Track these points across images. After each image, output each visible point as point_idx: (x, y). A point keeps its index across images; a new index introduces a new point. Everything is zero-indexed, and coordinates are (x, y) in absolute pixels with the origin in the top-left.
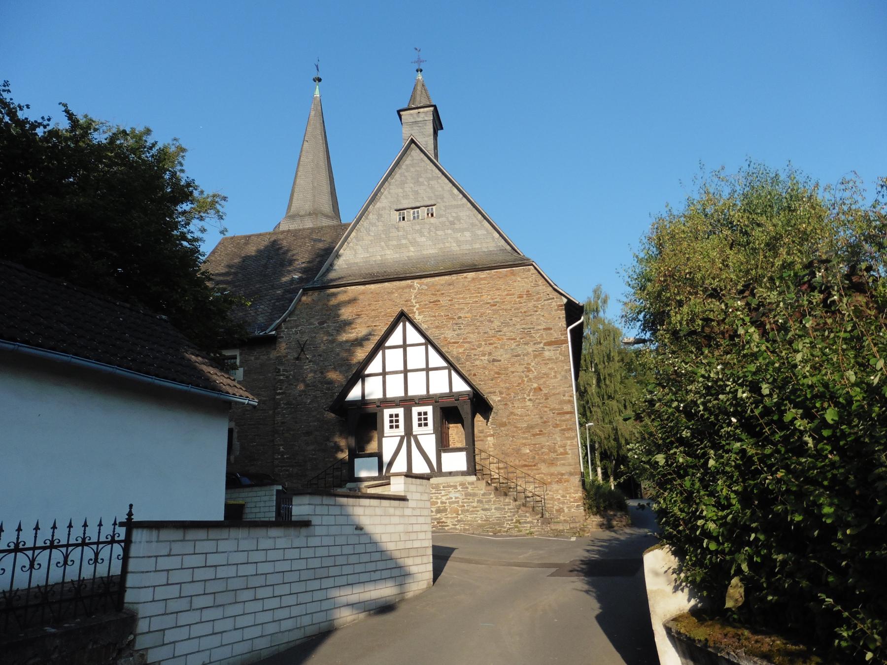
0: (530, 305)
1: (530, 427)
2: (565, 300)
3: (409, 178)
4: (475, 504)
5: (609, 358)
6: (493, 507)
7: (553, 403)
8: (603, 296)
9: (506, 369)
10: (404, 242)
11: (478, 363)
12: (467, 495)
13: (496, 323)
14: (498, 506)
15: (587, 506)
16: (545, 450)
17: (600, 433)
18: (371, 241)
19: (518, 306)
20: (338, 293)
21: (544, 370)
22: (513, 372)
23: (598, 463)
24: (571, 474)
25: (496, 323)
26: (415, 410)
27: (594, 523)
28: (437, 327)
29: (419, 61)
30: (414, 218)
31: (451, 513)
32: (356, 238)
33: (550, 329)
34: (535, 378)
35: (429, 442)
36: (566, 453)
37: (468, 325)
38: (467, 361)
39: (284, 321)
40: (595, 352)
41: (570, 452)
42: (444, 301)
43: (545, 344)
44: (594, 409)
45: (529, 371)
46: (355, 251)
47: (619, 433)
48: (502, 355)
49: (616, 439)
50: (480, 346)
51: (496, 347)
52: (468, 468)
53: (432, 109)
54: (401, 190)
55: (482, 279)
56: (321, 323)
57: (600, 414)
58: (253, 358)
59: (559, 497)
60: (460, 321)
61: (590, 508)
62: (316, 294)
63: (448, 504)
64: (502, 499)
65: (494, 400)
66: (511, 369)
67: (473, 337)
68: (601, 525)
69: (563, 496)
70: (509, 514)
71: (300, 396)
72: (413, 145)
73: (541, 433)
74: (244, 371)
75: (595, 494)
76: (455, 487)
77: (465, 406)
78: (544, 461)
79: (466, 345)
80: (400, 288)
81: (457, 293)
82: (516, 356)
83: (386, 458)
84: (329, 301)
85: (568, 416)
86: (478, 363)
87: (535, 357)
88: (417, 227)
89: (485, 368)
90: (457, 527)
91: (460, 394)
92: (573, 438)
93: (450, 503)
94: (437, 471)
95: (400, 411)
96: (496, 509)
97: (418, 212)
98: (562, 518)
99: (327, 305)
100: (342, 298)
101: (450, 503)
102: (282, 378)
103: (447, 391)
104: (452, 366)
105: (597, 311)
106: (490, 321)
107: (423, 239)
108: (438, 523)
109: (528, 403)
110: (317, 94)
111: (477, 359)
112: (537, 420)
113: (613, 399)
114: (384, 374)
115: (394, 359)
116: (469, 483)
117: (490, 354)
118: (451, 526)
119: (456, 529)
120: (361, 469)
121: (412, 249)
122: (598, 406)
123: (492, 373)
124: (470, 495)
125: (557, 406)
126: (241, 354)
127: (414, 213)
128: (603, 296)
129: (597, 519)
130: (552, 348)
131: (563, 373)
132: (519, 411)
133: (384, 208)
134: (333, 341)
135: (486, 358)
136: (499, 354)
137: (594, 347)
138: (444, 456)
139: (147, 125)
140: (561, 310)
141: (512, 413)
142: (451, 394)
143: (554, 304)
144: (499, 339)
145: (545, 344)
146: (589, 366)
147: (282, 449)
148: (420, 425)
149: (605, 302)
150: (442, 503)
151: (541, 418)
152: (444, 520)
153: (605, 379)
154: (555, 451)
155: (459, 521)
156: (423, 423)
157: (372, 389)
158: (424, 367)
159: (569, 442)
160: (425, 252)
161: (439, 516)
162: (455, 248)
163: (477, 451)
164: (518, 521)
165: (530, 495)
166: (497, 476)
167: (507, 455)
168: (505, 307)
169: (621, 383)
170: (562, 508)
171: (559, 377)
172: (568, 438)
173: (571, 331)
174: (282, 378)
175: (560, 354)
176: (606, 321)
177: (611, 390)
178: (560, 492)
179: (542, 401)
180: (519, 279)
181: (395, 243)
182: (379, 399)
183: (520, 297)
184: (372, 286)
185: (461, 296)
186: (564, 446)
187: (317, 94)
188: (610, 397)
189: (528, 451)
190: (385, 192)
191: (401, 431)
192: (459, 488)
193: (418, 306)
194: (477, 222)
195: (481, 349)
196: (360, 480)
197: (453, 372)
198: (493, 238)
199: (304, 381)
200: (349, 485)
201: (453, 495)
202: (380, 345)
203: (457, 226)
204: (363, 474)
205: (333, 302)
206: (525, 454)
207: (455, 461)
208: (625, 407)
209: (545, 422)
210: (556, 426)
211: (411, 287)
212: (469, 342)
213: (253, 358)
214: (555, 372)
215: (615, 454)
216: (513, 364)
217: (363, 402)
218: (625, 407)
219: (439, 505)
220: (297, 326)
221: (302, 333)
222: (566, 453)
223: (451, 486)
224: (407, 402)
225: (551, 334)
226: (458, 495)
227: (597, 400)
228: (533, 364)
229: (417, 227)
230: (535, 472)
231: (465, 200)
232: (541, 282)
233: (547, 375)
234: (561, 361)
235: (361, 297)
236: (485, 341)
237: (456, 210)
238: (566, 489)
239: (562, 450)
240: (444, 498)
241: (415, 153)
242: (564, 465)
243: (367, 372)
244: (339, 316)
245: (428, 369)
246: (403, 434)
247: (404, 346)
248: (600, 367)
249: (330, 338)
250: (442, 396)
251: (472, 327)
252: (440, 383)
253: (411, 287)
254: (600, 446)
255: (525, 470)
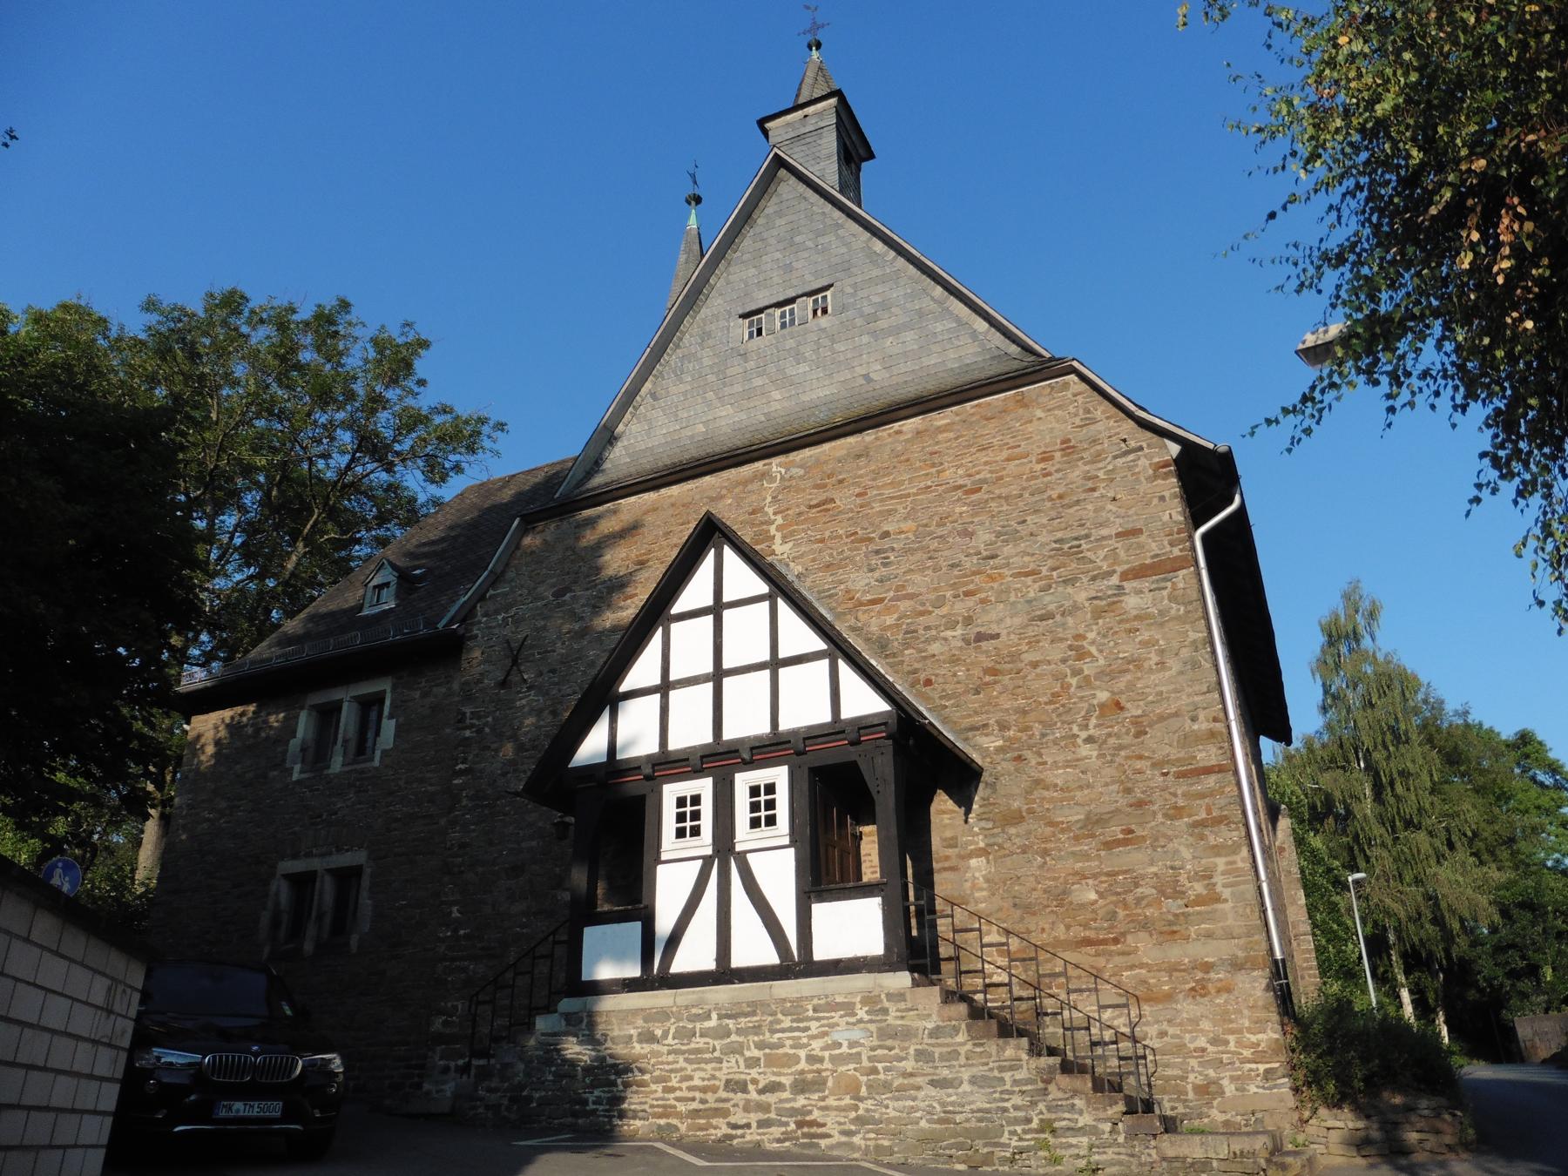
0: (1076, 474)
1: (1093, 822)
2: (1175, 449)
3: (773, 241)
4: (909, 1065)
5: (1399, 738)
6: (966, 1076)
7: (1160, 743)
8: (1365, 605)
9: (1015, 657)
10: (758, 382)
11: (935, 648)
12: (886, 1033)
13: (983, 537)
14: (979, 1070)
15: (1300, 1074)
16: (1145, 890)
17: (1396, 907)
18: (685, 393)
19: (1039, 483)
20: (599, 517)
21: (1128, 649)
22: (1035, 665)
23: (1401, 978)
24: (1237, 966)
25: (983, 537)
26: (743, 781)
27: (1334, 1136)
28: (828, 566)
29: (816, 27)
30: (783, 325)
31: (839, 1091)
32: (654, 396)
33: (1136, 532)
34: (1101, 674)
35: (777, 870)
36: (1218, 899)
37: (908, 551)
38: (907, 645)
39: (481, 598)
40: (1362, 723)
41: (1226, 893)
42: (844, 499)
43: (1125, 576)
44: (1374, 852)
45: (1080, 658)
46: (649, 421)
47: (1443, 905)
48: (1003, 620)
49: (1438, 921)
50: (940, 602)
51: (983, 601)
52: (887, 946)
53: (833, 101)
54: (753, 271)
55: (940, 430)
56: (559, 594)
57: (1388, 862)
58: (417, 694)
59: (1202, 1042)
60: (886, 544)
61: (1315, 1079)
62: (553, 526)
63: (827, 1065)
64: (992, 1046)
65: (981, 748)
66: (1028, 657)
67: (920, 582)
68: (1360, 1144)
69: (1215, 1041)
70: (1017, 1100)
71: (504, 774)
72: (783, 172)
73: (1129, 839)
74: (398, 727)
75: (1330, 1034)
76: (849, 1008)
77: (879, 760)
78: (1145, 925)
79: (904, 605)
80: (738, 483)
81: (876, 474)
82: (1042, 618)
83: (664, 923)
84: (578, 539)
85: (1211, 781)
86: (935, 648)
87: (1098, 614)
88: (791, 343)
89: (954, 660)
90: (857, 1140)
91: (863, 725)
92: (1234, 850)
93: (833, 1059)
94: (798, 963)
95: (704, 787)
96: (973, 1081)
97: (792, 312)
98: (1217, 1116)
99: (573, 549)
100: (608, 526)
101: (833, 1059)
102: (467, 733)
103: (826, 717)
104: (838, 648)
105: (1356, 637)
106: (968, 534)
107: (804, 368)
108: (800, 1125)
109: (1086, 750)
110: (693, 223)
111: (935, 639)
112: (1112, 798)
113: (1418, 827)
114: (665, 687)
115: (689, 645)
116: (889, 996)
117: (968, 621)
118: (838, 1138)
119: (851, 1146)
120: (598, 958)
121: (776, 395)
122: (1383, 845)
123: (977, 672)
124: (894, 1036)
125: (1175, 753)
126: (394, 688)
127: (783, 316)
128: (1365, 605)
129: (1344, 1121)
130: (1145, 584)
131: (1185, 653)
132: (1059, 776)
133: (716, 317)
134: (584, 632)
135: (959, 632)
136: (995, 618)
137: (1358, 714)
138: (820, 910)
139: (342, 295)
140: (1166, 476)
141: (1038, 782)
142: (837, 729)
143: (1143, 462)
144: (992, 578)
145: (1125, 576)
146: (1352, 757)
147: (455, 914)
148: (755, 823)
149: (1372, 615)
150: (811, 1059)
151: (1128, 791)
152: (816, 1115)
153: (1392, 784)
154: (1178, 894)
155: (860, 1121)
156: (763, 818)
157: (634, 730)
158: (782, 671)
159: (1221, 863)
160: (805, 398)
161: (801, 1101)
162: (879, 374)
163: (939, 905)
164: (1047, 1126)
165: (1108, 1035)
166: (1004, 978)
167: (1029, 909)
168: (1004, 491)
169: (1433, 792)
170: (1216, 1082)
171: (1175, 666)
172: (1217, 850)
173: (1205, 537)
174: (467, 733)
175: (1172, 598)
176: (1380, 657)
177: (1409, 808)
178: (1205, 1025)
179: (1127, 740)
180: (1039, 413)
181: (738, 388)
182: (649, 757)
183: (1046, 458)
184: (675, 490)
185: (888, 480)
186: (1207, 876)
187: (693, 223)
188: (1409, 824)
189: (1093, 896)
190: (718, 281)
191: (704, 843)
192: (862, 1013)
193: (779, 520)
194: (933, 306)
195: (944, 610)
196: (598, 989)
197: (842, 664)
198: (974, 335)
199: (514, 737)
200: (566, 1005)
201: (842, 1035)
202: (657, 613)
203: (883, 324)
204: (605, 972)
205: (590, 537)
206: (1082, 906)
207: (853, 926)
208: (1451, 846)
209: (1140, 804)
210: (1176, 813)
211: (764, 475)
212: (911, 597)
213: (417, 694)
214: (1161, 652)
215: (1440, 954)
216: (1033, 643)
217: (613, 767)
218: (1451, 846)
219: (803, 1065)
220: (507, 608)
221: (517, 621)
222: (1218, 899)
223: (834, 1007)
224: (721, 760)
225: (1140, 546)
226: (856, 1034)
227: (1378, 831)
228: (1091, 636)
229: (791, 343)
230: (1118, 960)
231: (901, 260)
232: (1101, 409)
233: (1136, 662)
234: (1178, 618)
235: (649, 518)
236: (954, 586)
237: (880, 289)
238: (1224, 1017)
239: (1199, 888)
240: (816, 1045)
241: (788, 187)
242: (1209, 935)
243: (624, 687)
244: (598, 569)
245: (775, 664)
246: (709, 851)
247: (717, 609)
248: (1376, 756)
249: (577, 626)
250: (812, 735)
251: (919, 555)
252: (807, 700)
253: (764, 475)
254: (1400, 938)
255: (1085, 957)
